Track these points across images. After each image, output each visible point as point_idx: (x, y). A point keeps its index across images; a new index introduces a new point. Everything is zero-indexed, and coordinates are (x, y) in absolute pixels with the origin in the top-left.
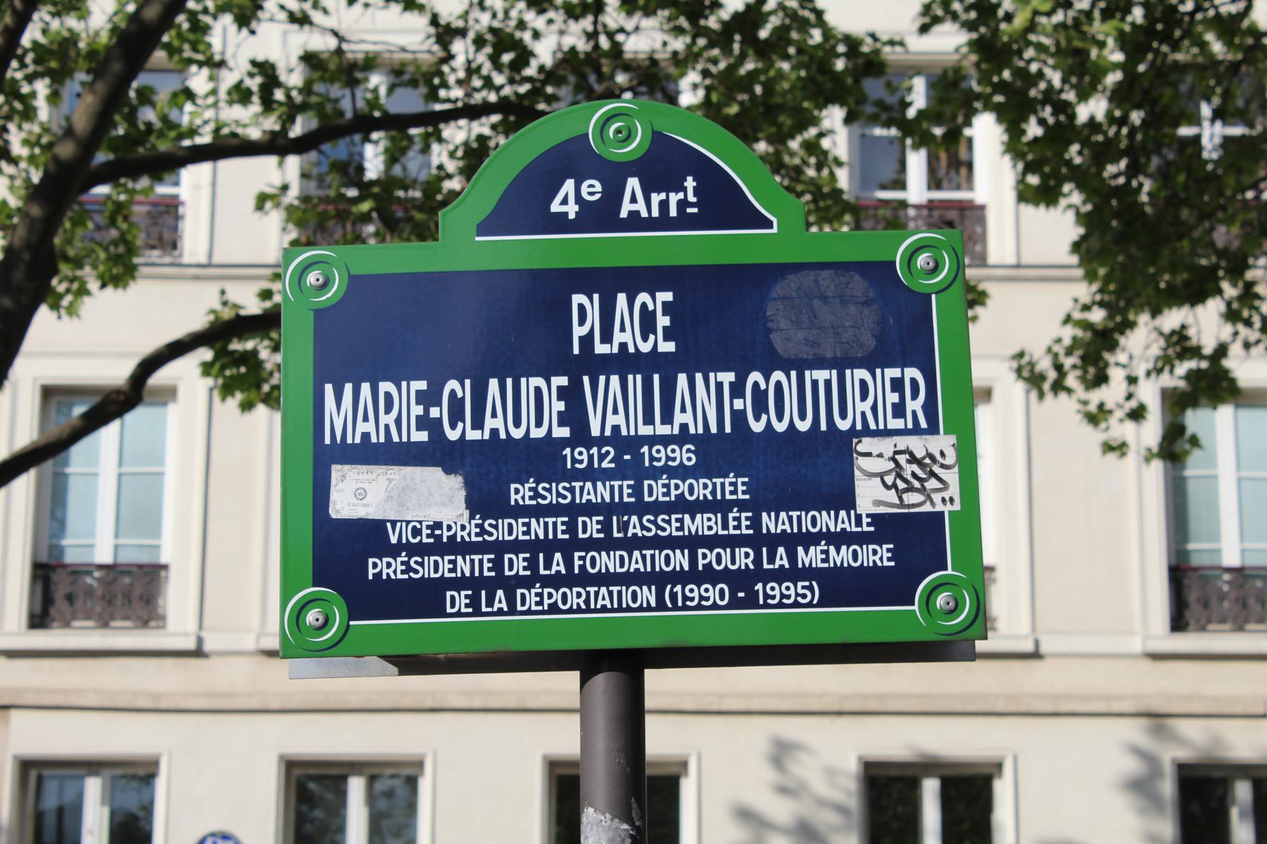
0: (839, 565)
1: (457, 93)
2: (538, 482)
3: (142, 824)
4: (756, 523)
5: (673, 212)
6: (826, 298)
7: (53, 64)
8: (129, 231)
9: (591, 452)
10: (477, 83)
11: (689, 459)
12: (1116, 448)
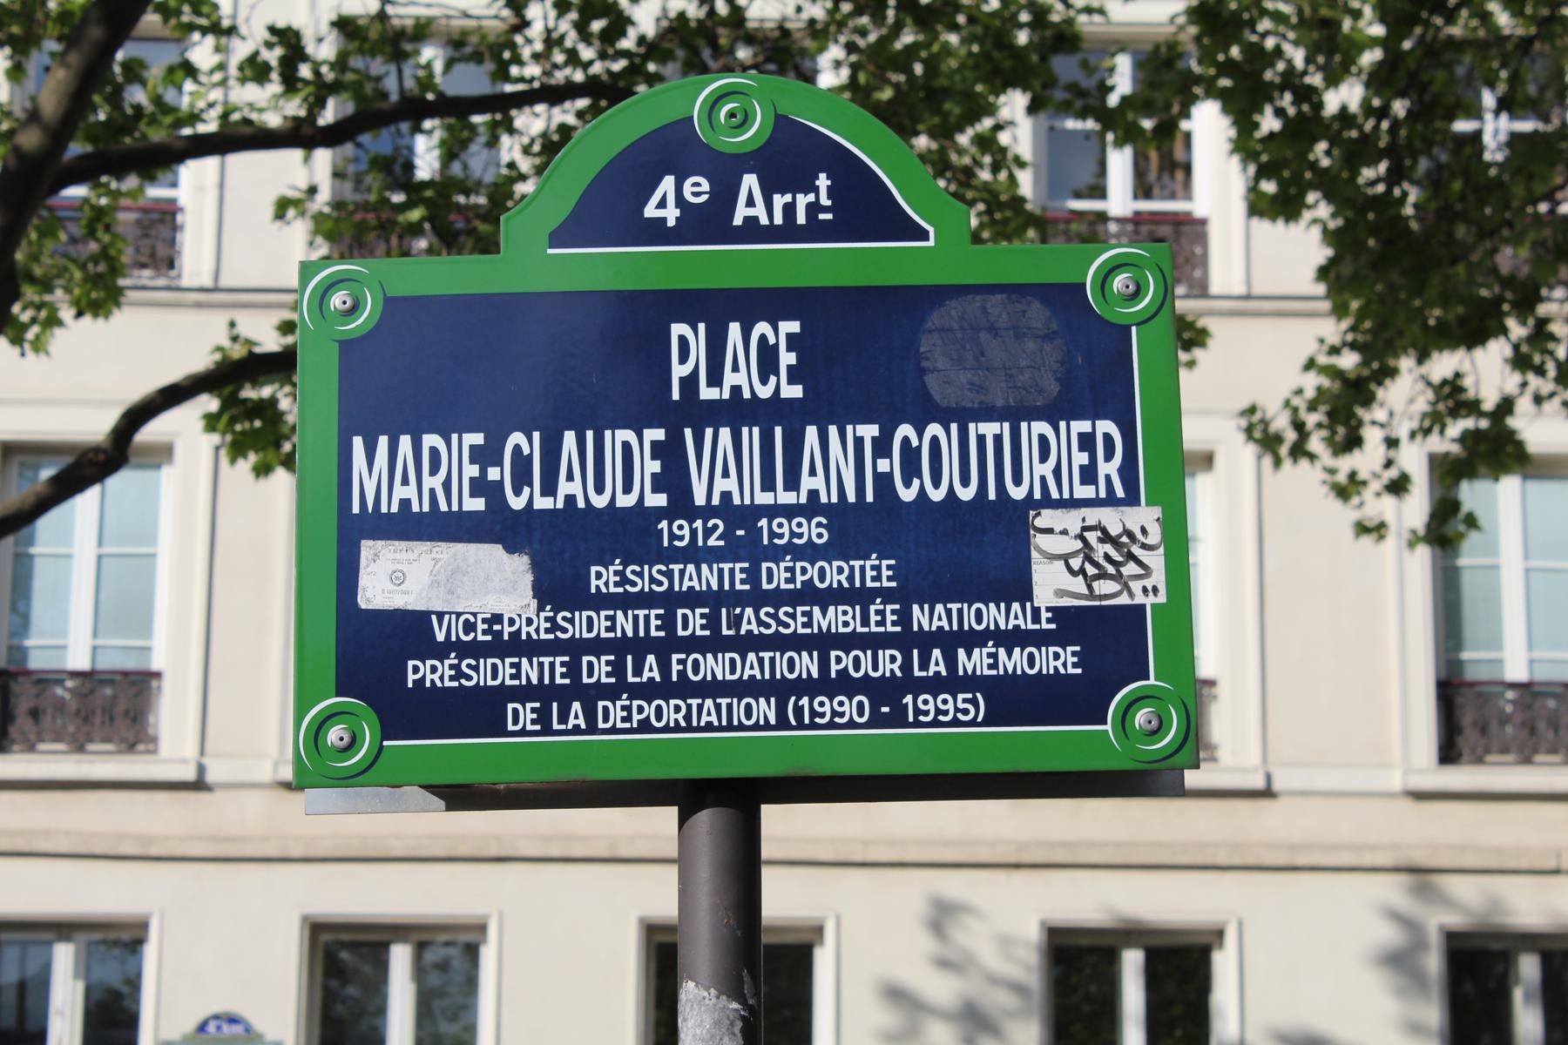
0: (1010, 673)
1: (533, 70)
2: (625, 564)
3: (127, 1003)
4: (904, 618)
5: (801, 219)
6: (996, 329)
7: (15, 29)
8: (112, 244)
9: (694, 526)
10: (559, 58)
11: (820, 536)
12: (1372, 530)
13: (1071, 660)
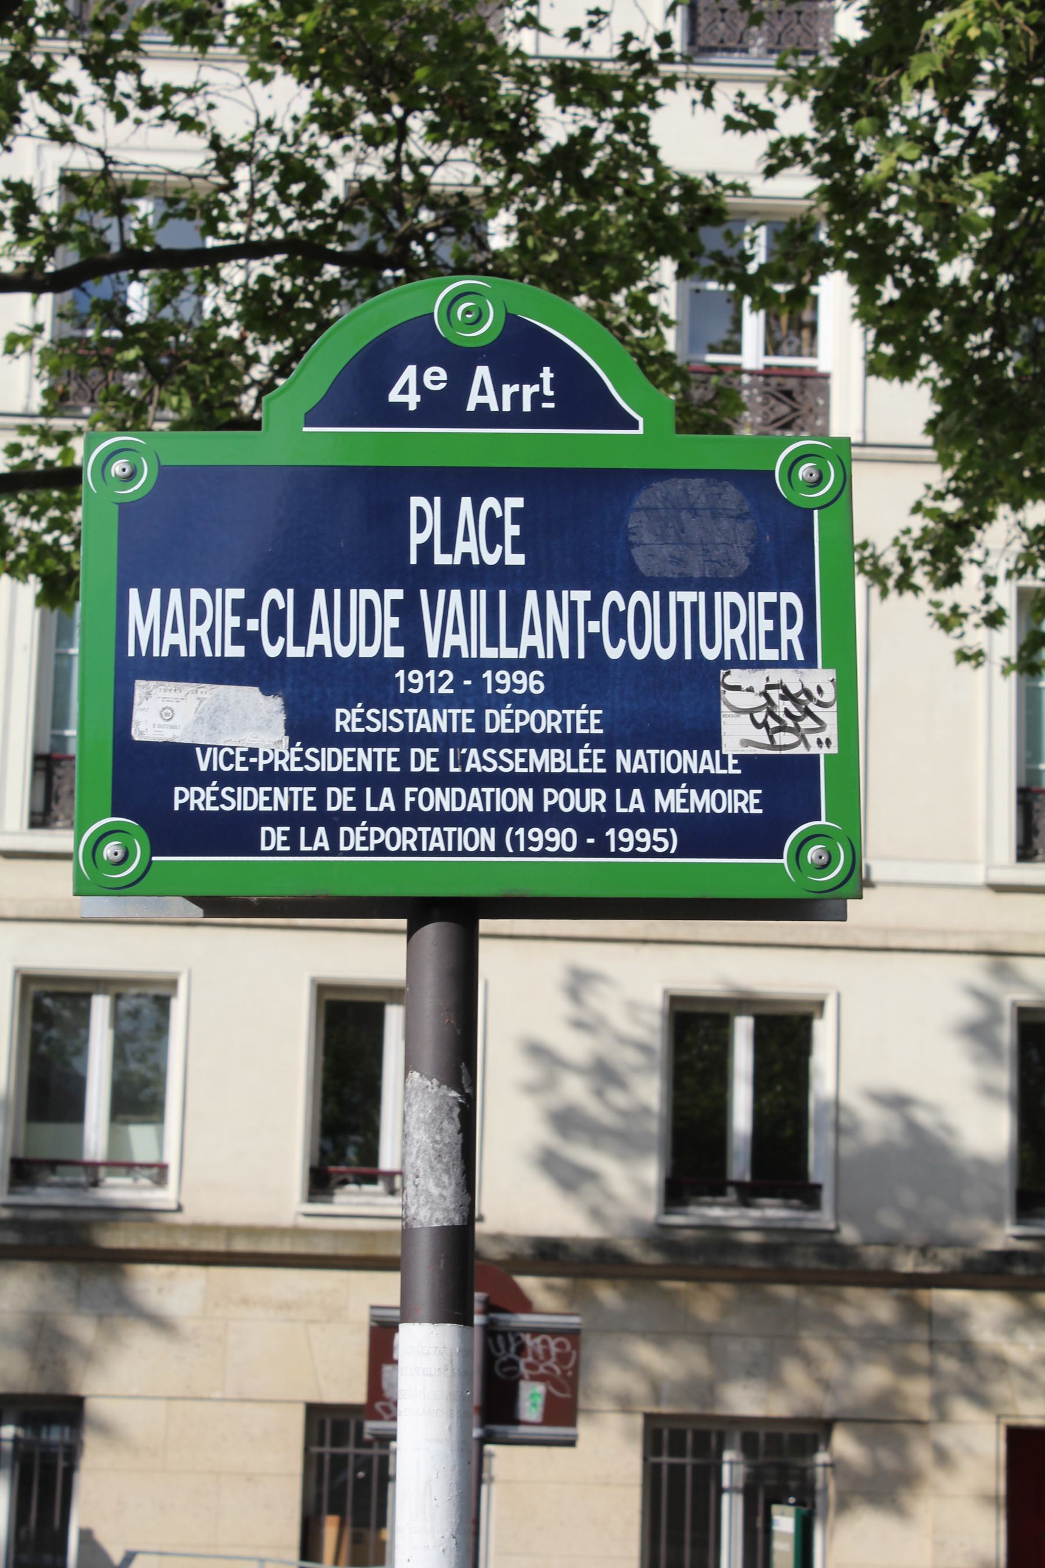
2: (366, 707)
4: (609, 761)
5: (527, 407)
9: (427, 675)
10: (261, 216)
11: (537, 687)
12: (970, 657)
13: (755, 801)
